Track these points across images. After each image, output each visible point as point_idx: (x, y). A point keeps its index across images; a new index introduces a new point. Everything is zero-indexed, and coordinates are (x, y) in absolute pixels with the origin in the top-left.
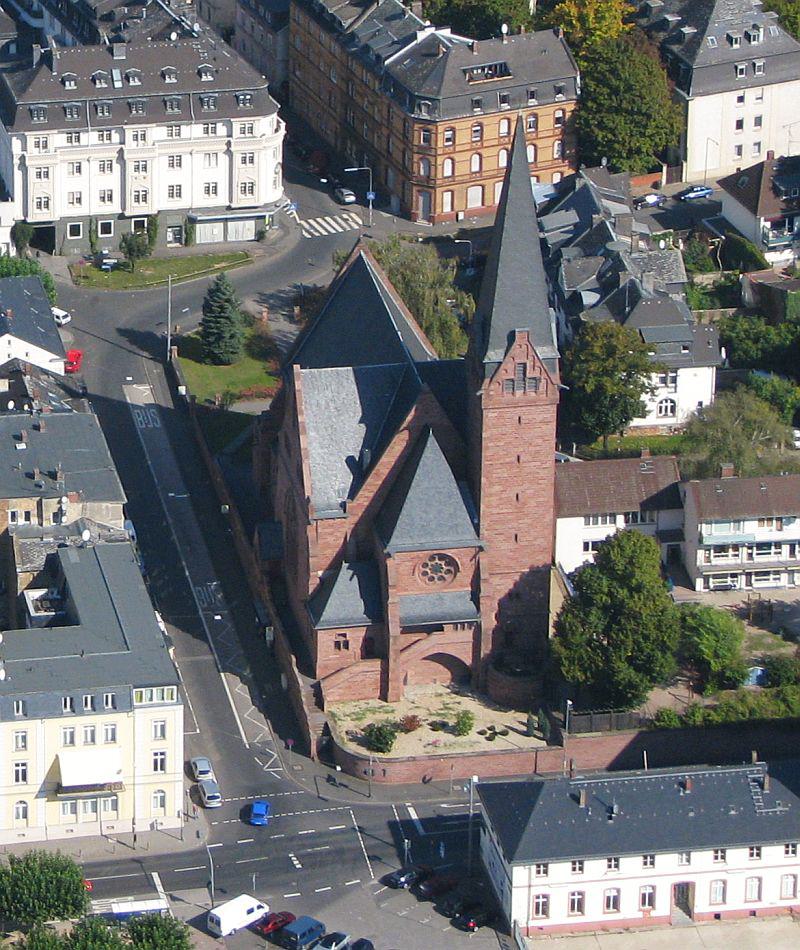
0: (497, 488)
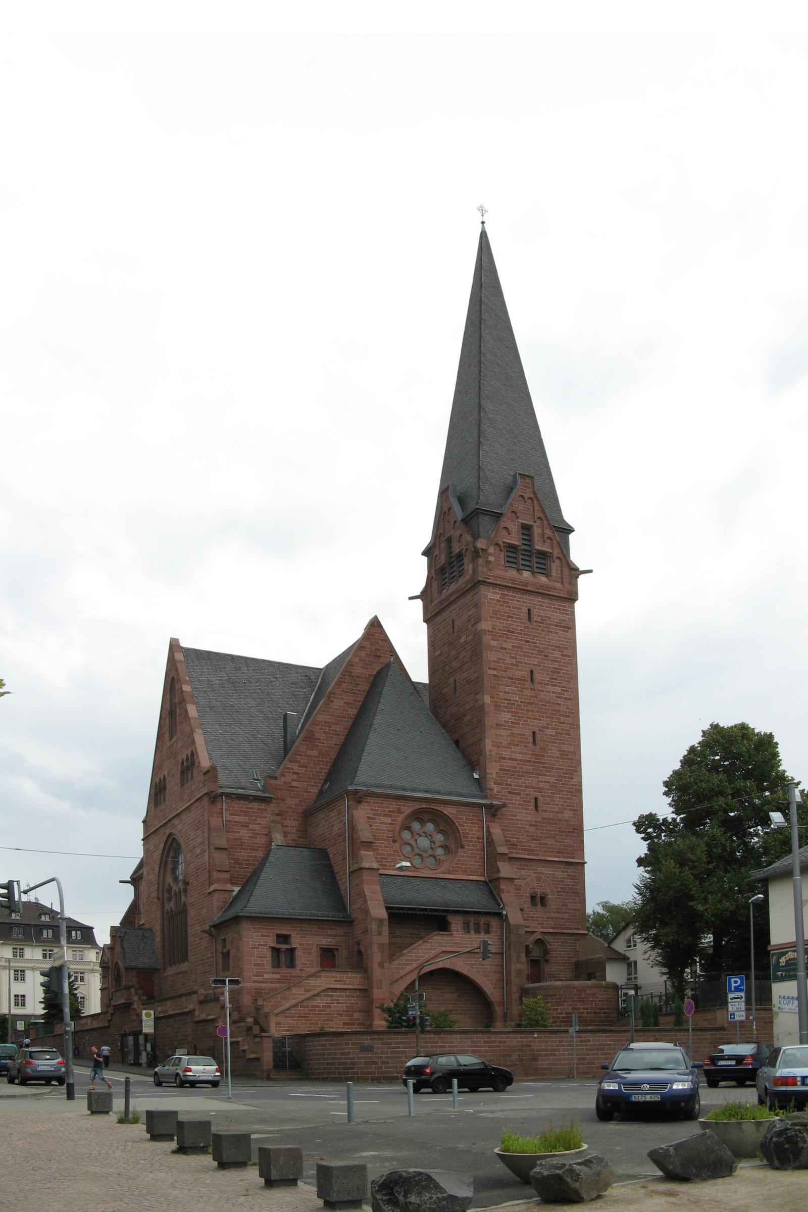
0: (506, 716)
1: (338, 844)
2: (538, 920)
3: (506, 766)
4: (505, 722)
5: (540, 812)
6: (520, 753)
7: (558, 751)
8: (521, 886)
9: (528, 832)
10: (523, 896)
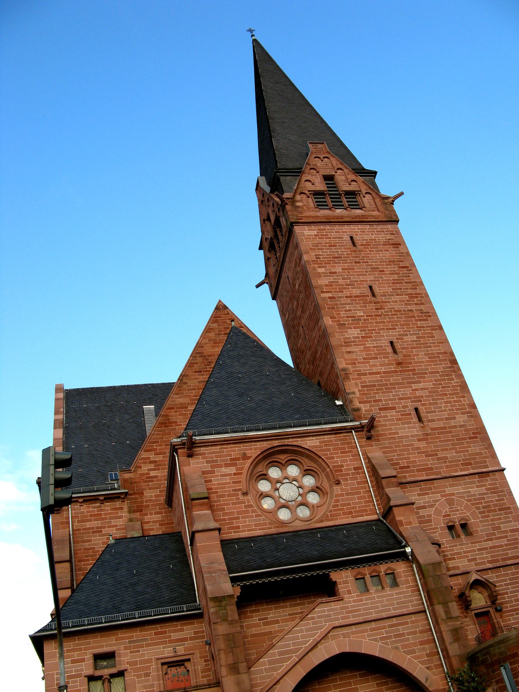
0: (353, 333)
2: (468, 556)
3: (369, 382)
6: (381, 365)
7: (426, 355)
8: (430, 516)
9: (418, 448)
10: (437, 528)
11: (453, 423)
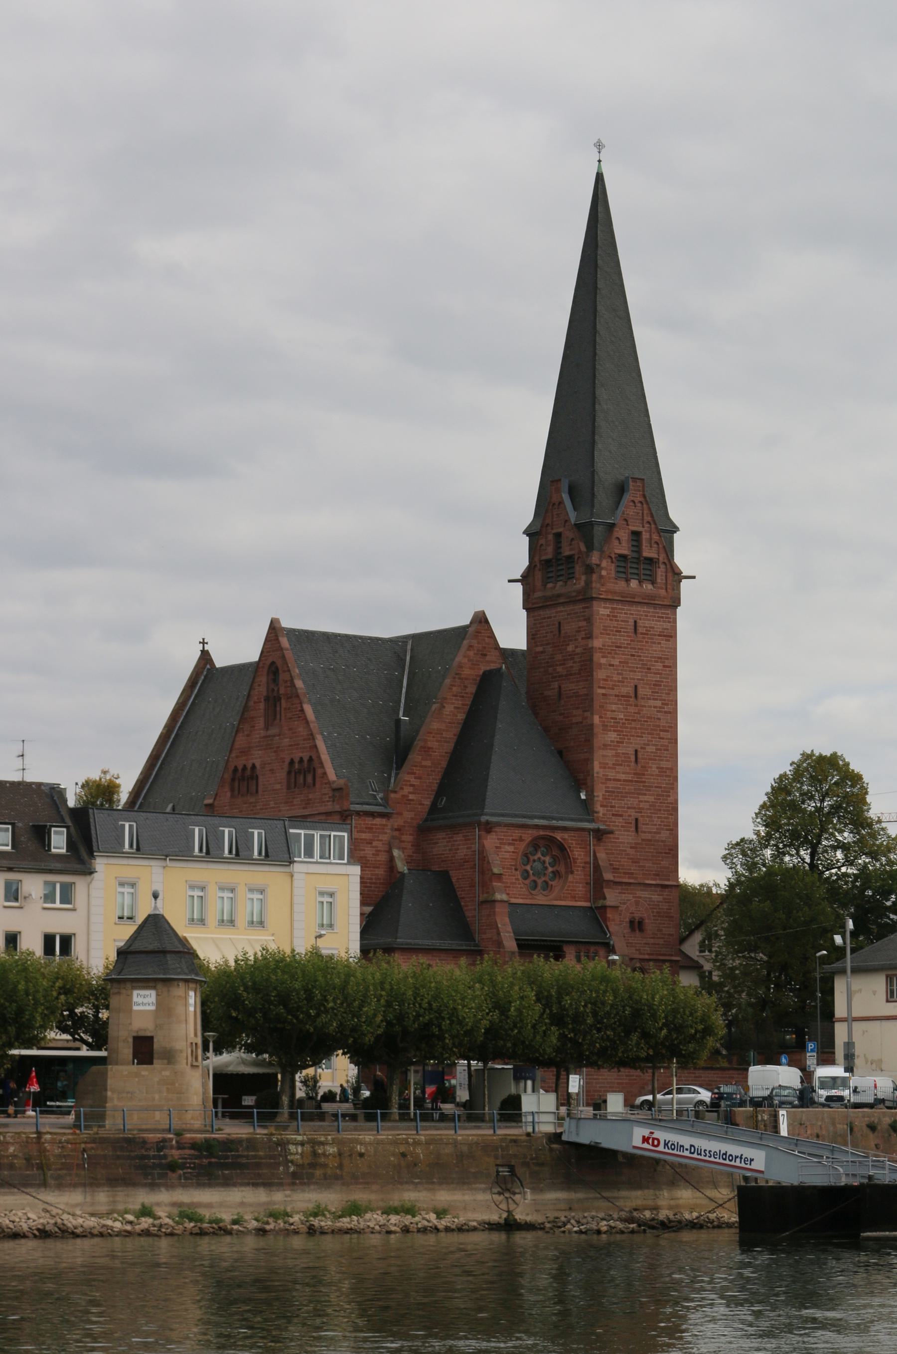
0: (612, 736)
1: (463, 869)
4: (612, 741)
5: (640, 834)
6: (624, 773)
9: (628, 854)
11: (657, 837)
